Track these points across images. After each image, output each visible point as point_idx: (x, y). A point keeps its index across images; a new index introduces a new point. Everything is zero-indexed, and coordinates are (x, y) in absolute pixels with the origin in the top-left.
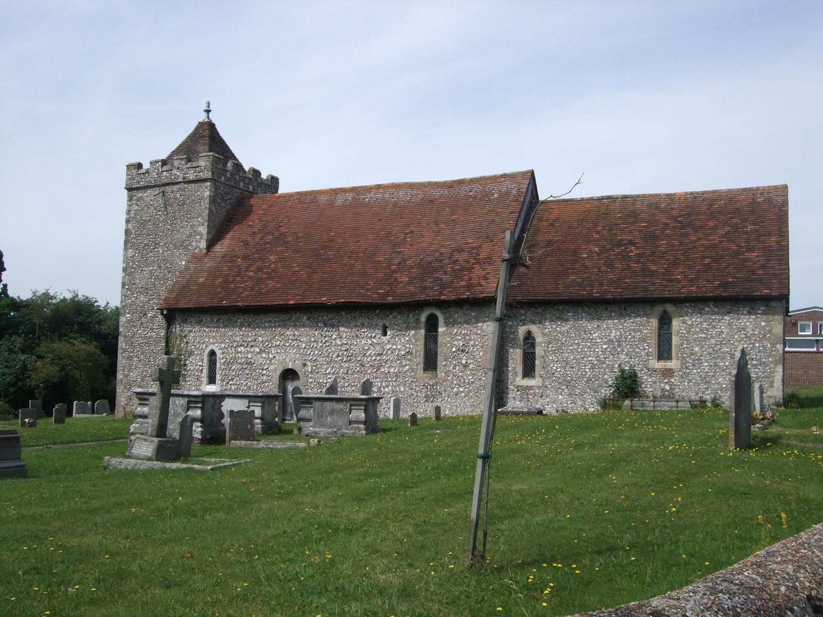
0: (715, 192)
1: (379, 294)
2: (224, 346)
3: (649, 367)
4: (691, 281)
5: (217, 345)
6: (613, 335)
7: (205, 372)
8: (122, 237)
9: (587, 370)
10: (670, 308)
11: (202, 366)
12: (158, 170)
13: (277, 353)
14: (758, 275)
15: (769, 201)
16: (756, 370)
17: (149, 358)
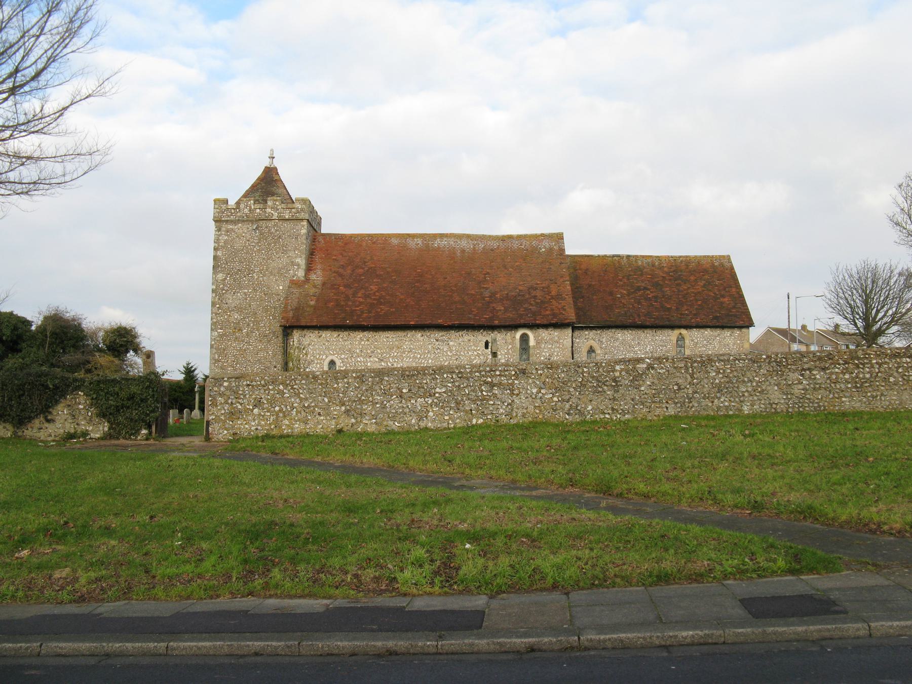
0: (687, 257)
1: (485, 318)
4: (695, 315)
8: (211, 263)
10: (684, 331)
12: (250, 207)
14: (733, 312)
15: (722, 265)
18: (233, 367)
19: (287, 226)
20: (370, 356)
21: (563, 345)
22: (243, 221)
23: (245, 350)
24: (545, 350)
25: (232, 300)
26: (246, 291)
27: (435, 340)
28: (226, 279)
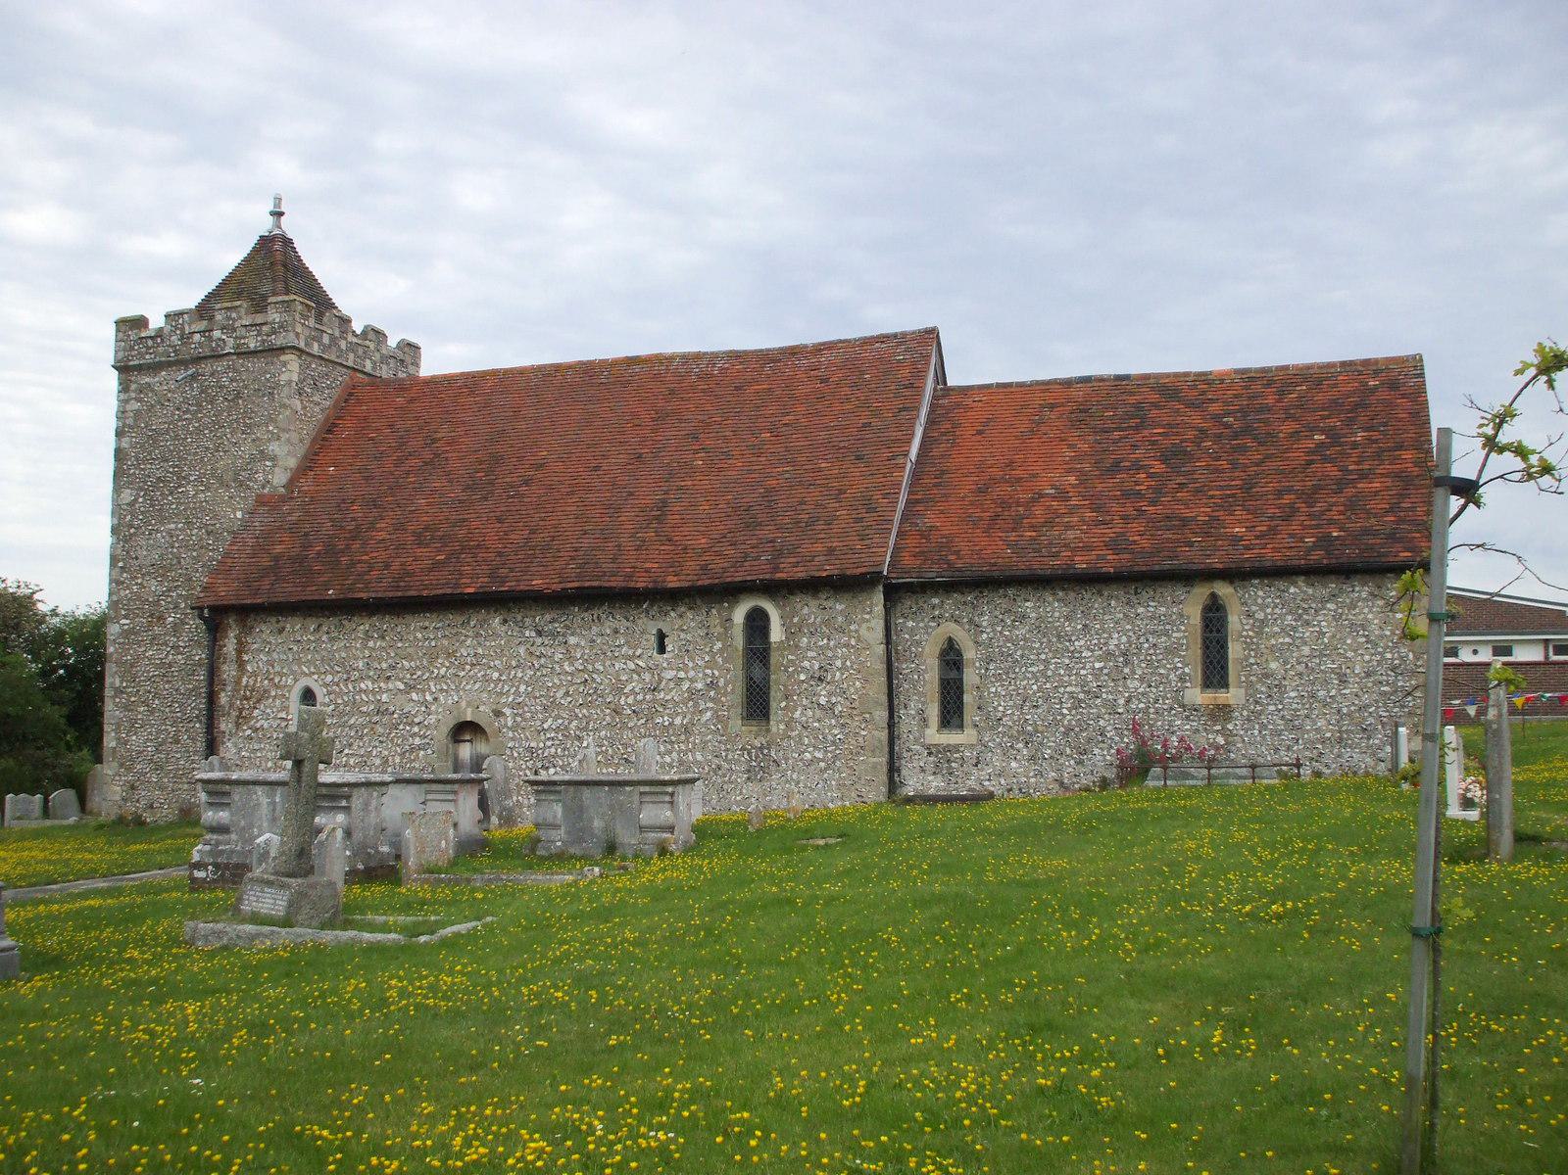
5: (316, 677)
9: (1065, 711)
10: (1223, 590)
12: (183, 329)
18: (147, 706)
19: (254, 367)
20: (389, 678)
21: (859, 640)
22: (169, 364)
24: (810, 654)
25: (147, 552)
26: (173, 526)
27: (533, 634)
28: (136, 500)
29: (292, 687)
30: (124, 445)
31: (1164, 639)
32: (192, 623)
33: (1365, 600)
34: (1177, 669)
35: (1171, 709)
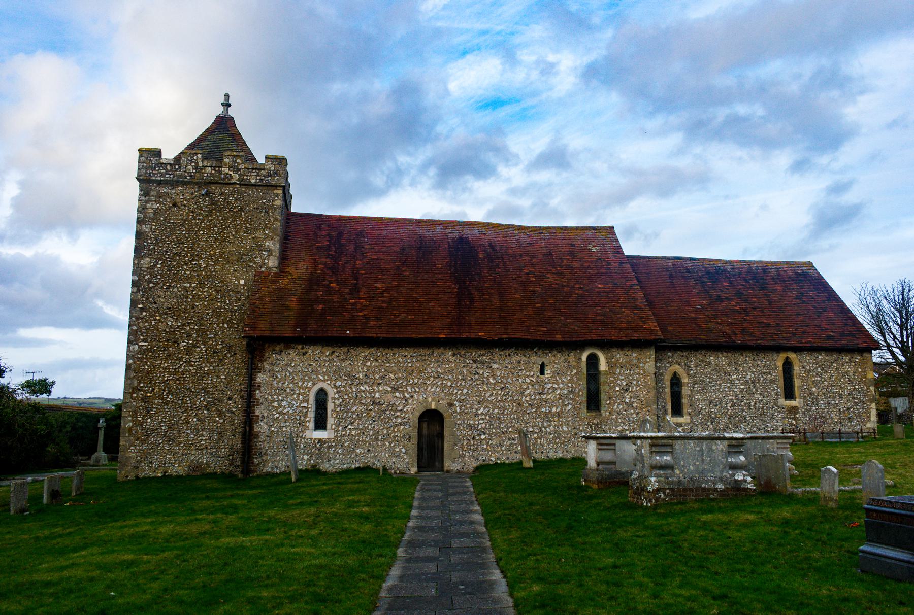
2: (340, 383)
3: (779, 404)
5: (329, 382)
6: (749, 377)
7: (311, 415)
9: (729, 408)
10: (792, 356)
11: (307, 408)
12: (197, 164)
13: (415, 391)
16: (858, 407)
17: (182, 399)
18: (162, 399)
20: (380, 384)
21: (644, 371)
23: (183, 373)
27: (471, 362)
29: (311, 388)
30: (146, 228)
31: (769, 376)
32: (202, 346)
33: (847, 363)
34: (775, 389)
35: (773, 408)
